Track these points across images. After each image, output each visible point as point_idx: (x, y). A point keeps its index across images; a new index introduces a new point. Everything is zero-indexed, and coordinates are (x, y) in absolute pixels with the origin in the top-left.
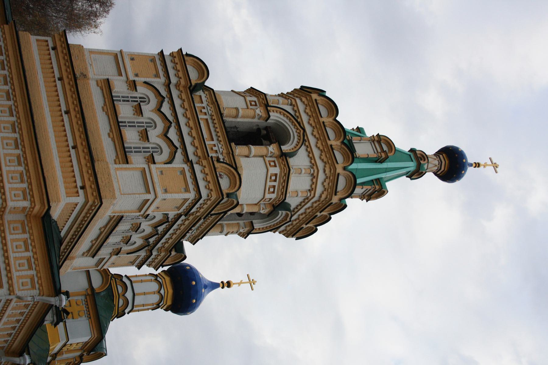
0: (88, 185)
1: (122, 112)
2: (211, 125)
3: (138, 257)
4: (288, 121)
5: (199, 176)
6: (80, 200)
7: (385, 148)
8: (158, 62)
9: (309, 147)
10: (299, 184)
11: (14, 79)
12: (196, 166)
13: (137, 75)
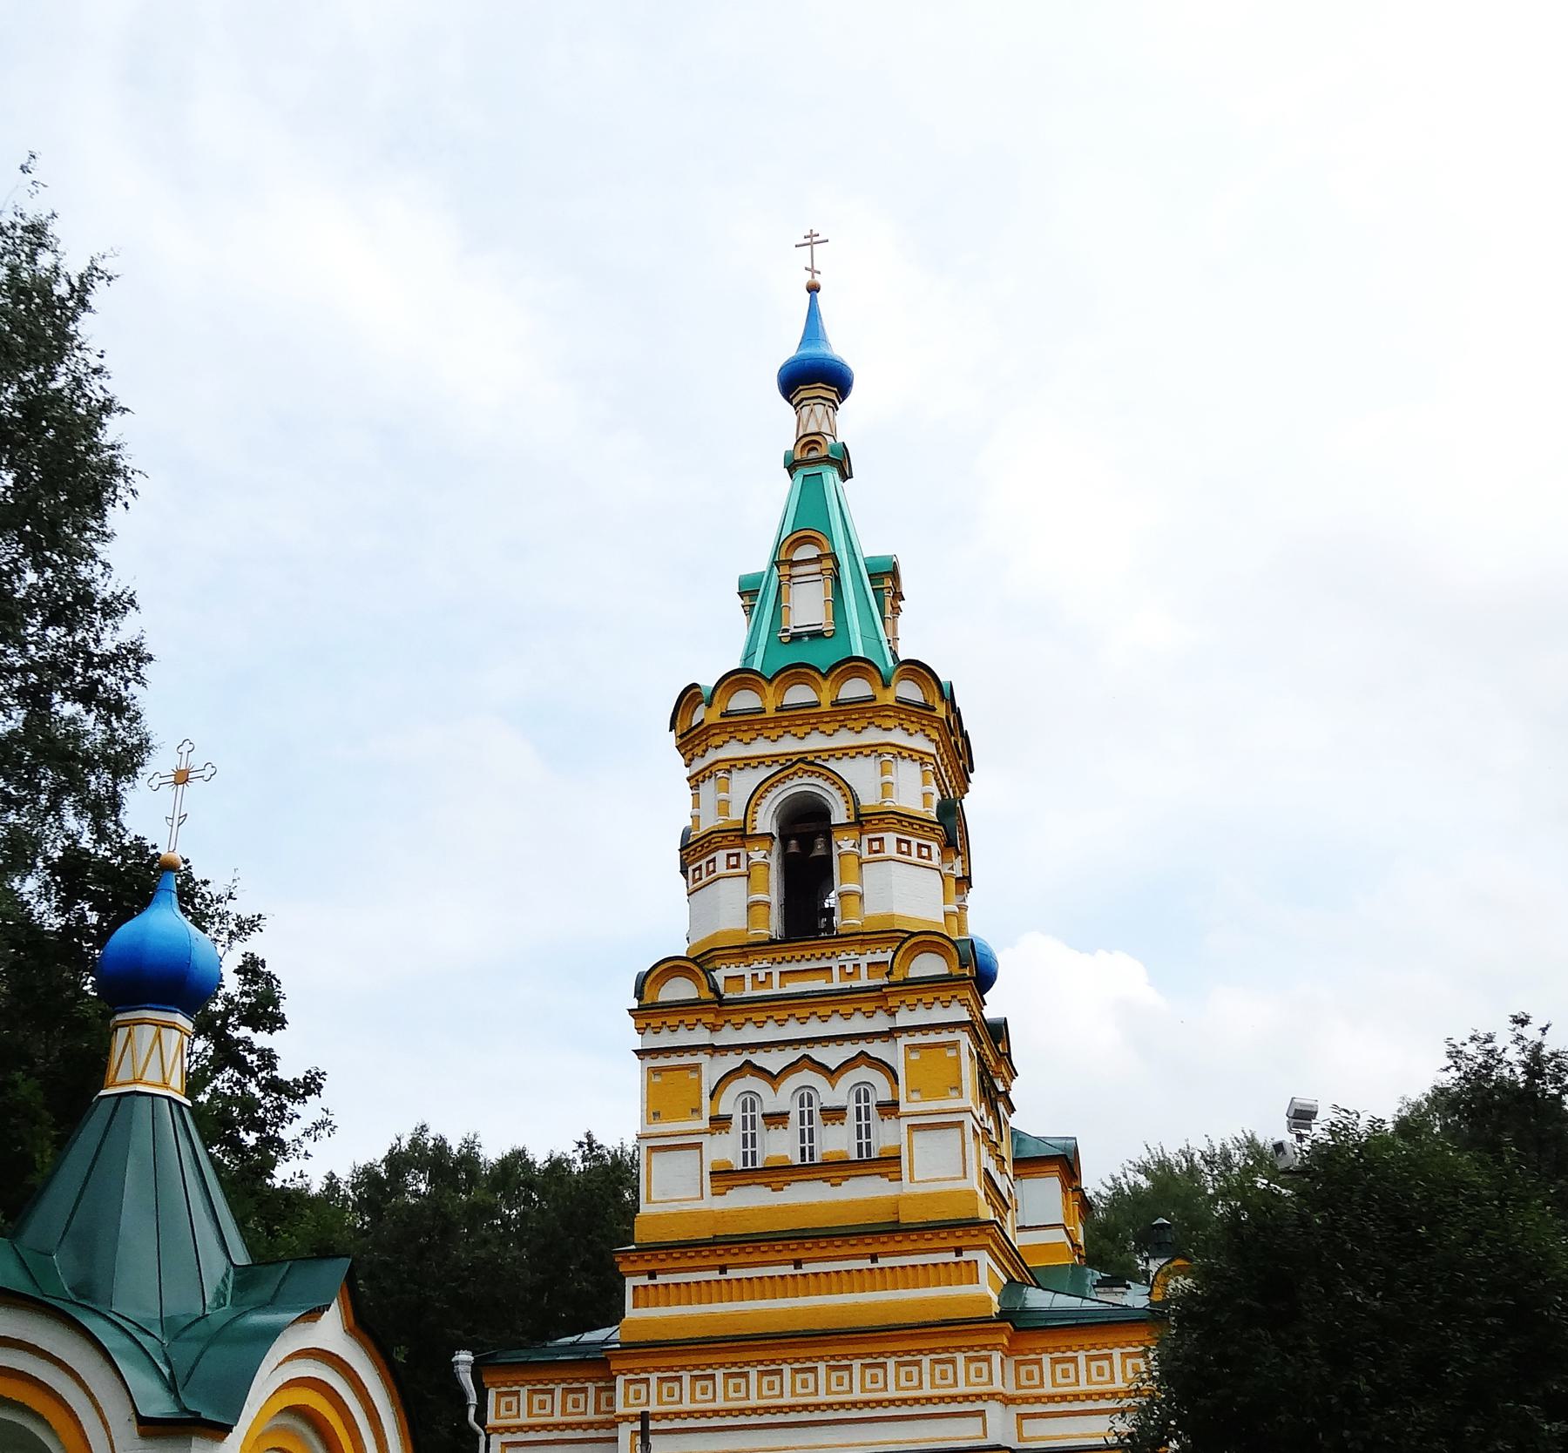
4: (775, 791)
5: (921, 1017)
8: (661, 1062)
9: (832, 753)
13: (697, 1111)
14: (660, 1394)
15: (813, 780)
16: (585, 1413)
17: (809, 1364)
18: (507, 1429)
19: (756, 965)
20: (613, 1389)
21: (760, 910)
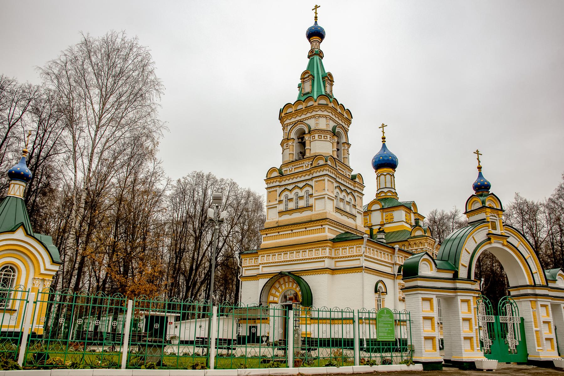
3: (357, 196)
5: (318, 174)
6: (327, 227)
7: (307, 76)
8: (270, 190)
10: (323, 124)
12: (314, 176)
18: (336, 258)
21: (291, 155)
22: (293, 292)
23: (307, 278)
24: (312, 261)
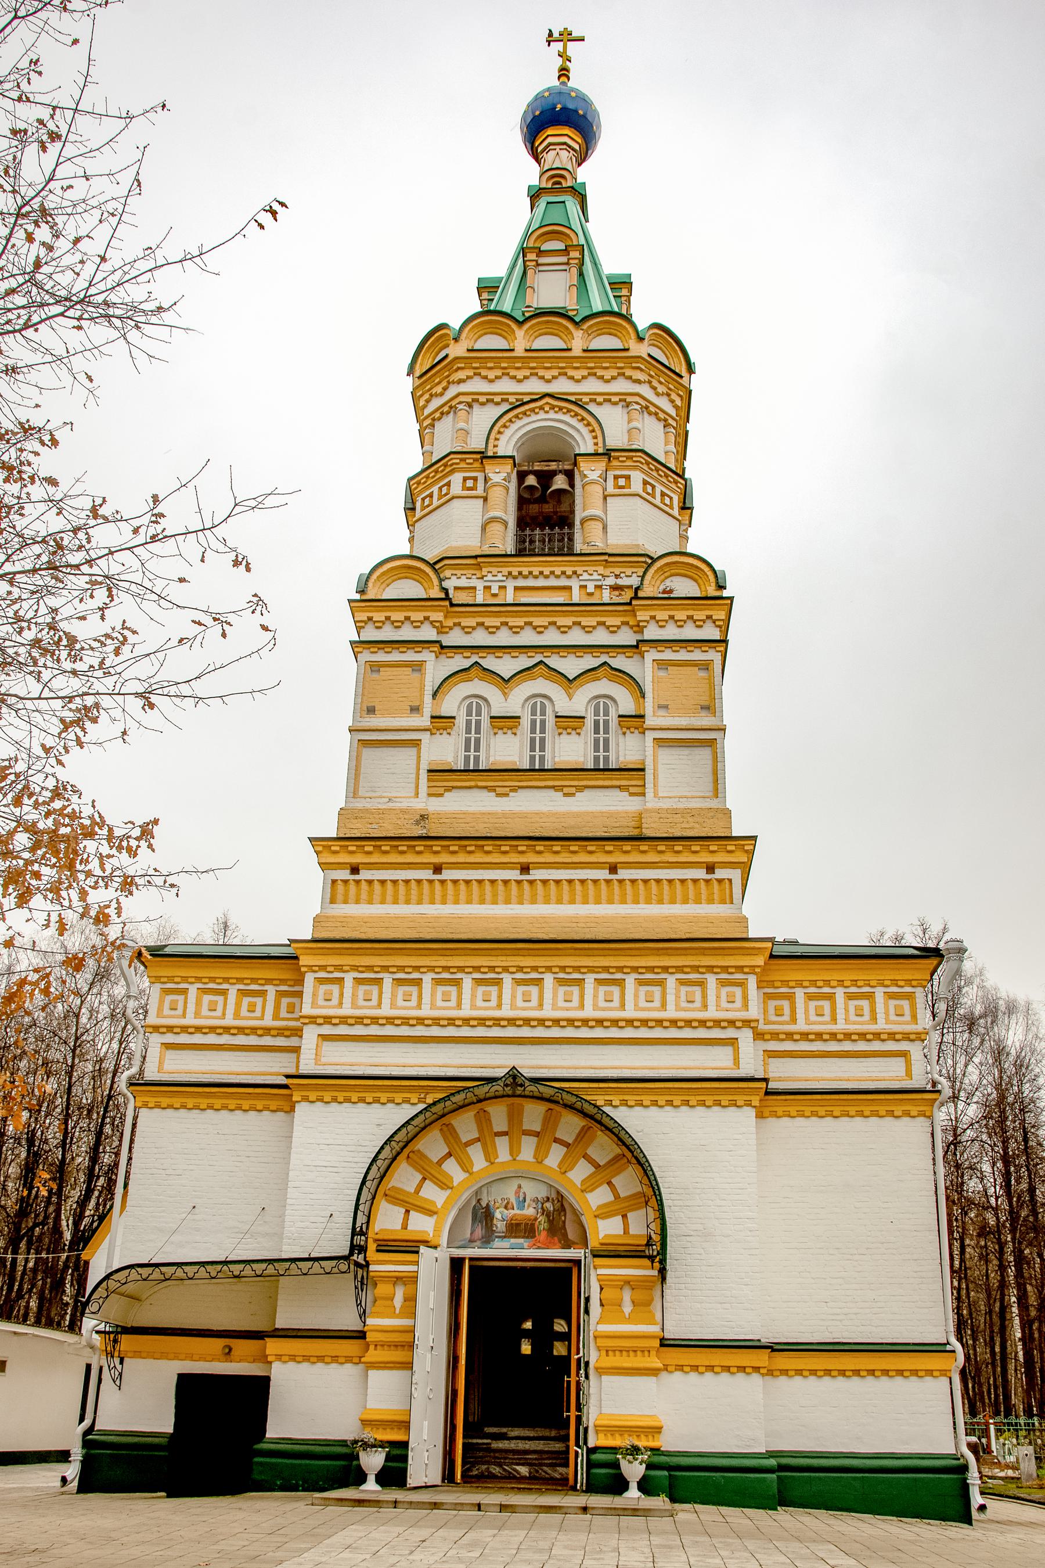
0: (706, 858)
1: (576, 758)
2: (531, 582)
4: (519, 423)
5: (671, 632)
11: (450, 964)
14: (354, 996)
15: (560, 416)
16: (262, 1018)
17: (534, 975)
19: (490, 577)
20: (300, 994)
22: (533, 1191)
23: (637, 1120)
24: (614, 1033)
